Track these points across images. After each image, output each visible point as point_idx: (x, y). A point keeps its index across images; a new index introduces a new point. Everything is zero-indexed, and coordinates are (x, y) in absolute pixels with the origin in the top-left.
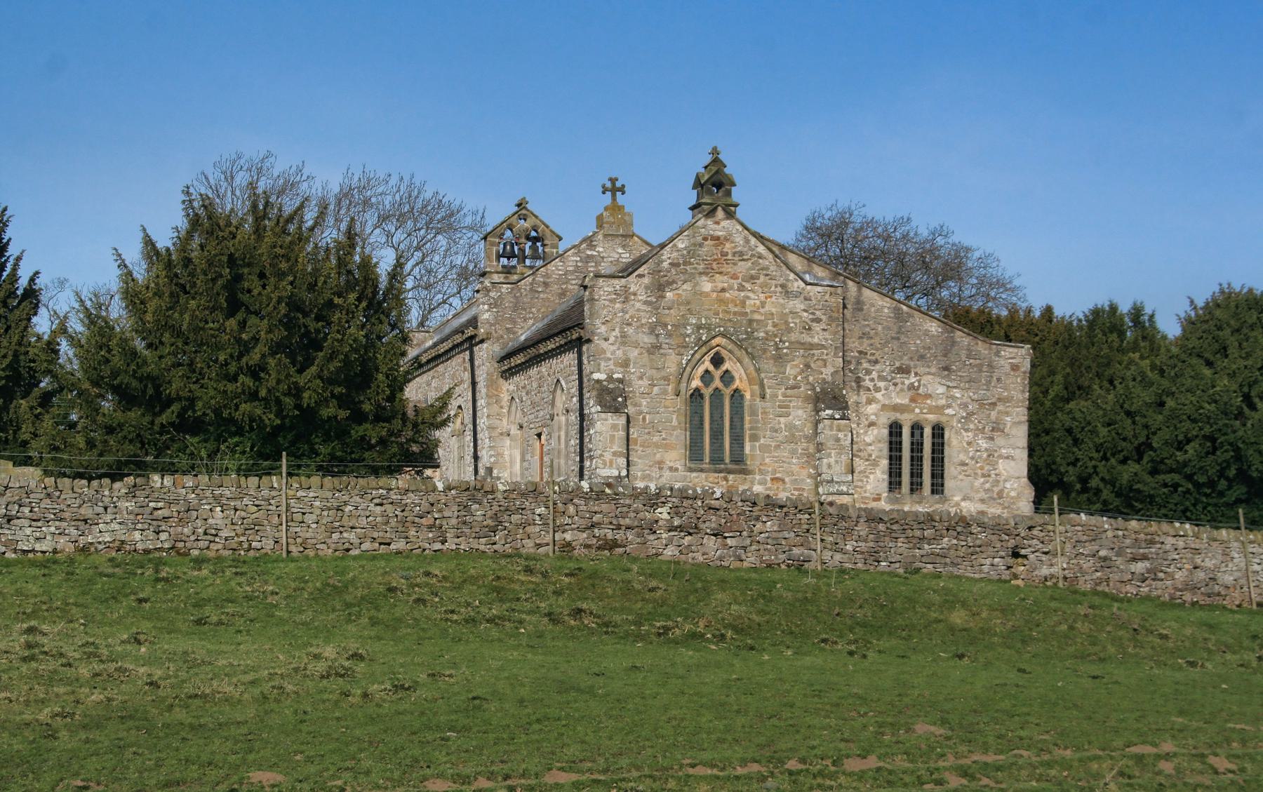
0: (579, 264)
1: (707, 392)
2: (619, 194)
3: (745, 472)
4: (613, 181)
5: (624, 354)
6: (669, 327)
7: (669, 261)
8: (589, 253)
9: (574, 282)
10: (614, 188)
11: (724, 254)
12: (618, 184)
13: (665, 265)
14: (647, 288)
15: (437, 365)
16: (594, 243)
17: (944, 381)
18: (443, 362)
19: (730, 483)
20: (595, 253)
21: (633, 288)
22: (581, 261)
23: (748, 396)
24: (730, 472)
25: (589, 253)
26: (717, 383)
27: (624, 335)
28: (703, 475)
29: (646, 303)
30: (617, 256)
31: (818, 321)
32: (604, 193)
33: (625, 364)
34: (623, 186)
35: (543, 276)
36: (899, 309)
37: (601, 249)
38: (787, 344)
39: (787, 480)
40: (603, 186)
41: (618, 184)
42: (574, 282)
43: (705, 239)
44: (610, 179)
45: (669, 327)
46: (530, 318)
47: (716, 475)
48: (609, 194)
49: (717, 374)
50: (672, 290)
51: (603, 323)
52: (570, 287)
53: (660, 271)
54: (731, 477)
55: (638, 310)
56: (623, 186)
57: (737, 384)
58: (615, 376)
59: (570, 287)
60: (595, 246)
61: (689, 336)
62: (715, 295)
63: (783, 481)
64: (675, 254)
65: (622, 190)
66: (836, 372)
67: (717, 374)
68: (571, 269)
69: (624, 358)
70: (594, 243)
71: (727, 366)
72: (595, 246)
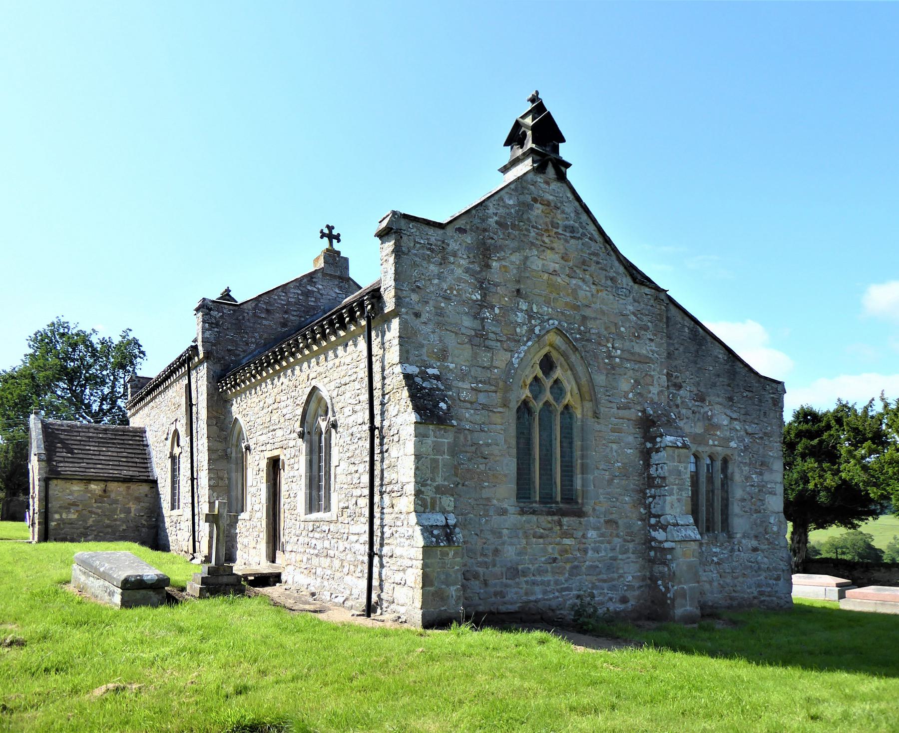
0: (301, 297)
1: (537, 406)
2: (335, 241)
3: (580, 514)
4: (330, 228)
5: (441, 341)
6: (497, 311)
7: (496, 218)
8: (309, 288)
9: (295, 313)
10: (330, 235)
11: (555, 225)
12: (335, 232)
13: (492, 221)
14: (468, 248)
15: (155, 397)
16: (314, 280)
17: (729, 412)
18: (160, 393)
19: (565, 528)
20: (315, 290)
21: (453, 246)
22: (302, 294)
23: (578, 414)
24: (564, 514)
25: (309, 288)
26: (548, 396)
27: (440, 312)
28: (534, 518)
29: (467, 271)
30: (334, 295)
31: (646, 329)
32: (322, 237)
33: (443, 355)
34: (339, 235)
35: (265, 303)
36: (697, 331)
37: (320, 287)
38: (619, 352)
39: (620, 522)
40: (322, 232)
41: (335, 232)
42: (295, 313)
43: (535, 200)
44: (328, 226)
45: (497, 311)
46: (252, 343)
47: (550, 518)
48: (326, 239)
49: (548, 383)
50: (499, 259)
51: (413, 290)
52: (292, 318)
53: (485, 230)
54: (565, 520)
55: (459, 279)
56: (339, 235)
57: (568, 398)
58: (430, 371)
59: (292, 318)
60: (315, 283)
61: (519, 325)
62: (546, 276)
63: (616, 523)
64: (501, 211)
65: (338, 237)
66: (662, 391)
67: (548, 383)
68: (293, 300)
69: (440, 346)
70: (314, 280)
71: (558, 373)
72: (315, 283)
